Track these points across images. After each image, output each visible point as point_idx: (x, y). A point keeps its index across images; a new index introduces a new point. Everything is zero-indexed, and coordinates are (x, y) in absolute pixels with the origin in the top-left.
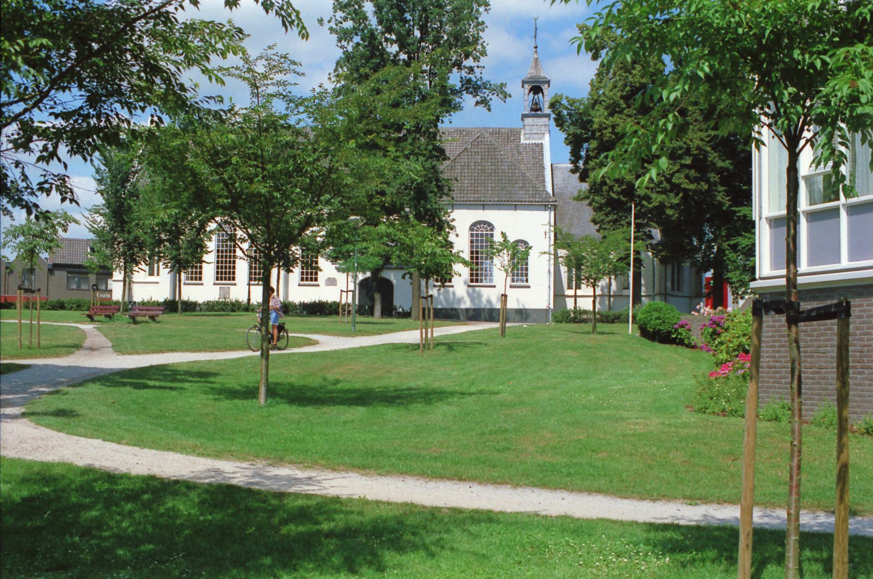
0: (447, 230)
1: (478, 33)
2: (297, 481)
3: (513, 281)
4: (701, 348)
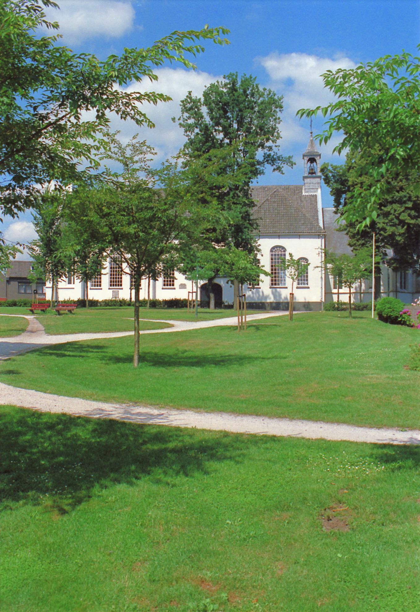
0: (256, 252)
1: (275, 125)
2: (152, 416)
3: (298, 284)
4: (417, 327)
